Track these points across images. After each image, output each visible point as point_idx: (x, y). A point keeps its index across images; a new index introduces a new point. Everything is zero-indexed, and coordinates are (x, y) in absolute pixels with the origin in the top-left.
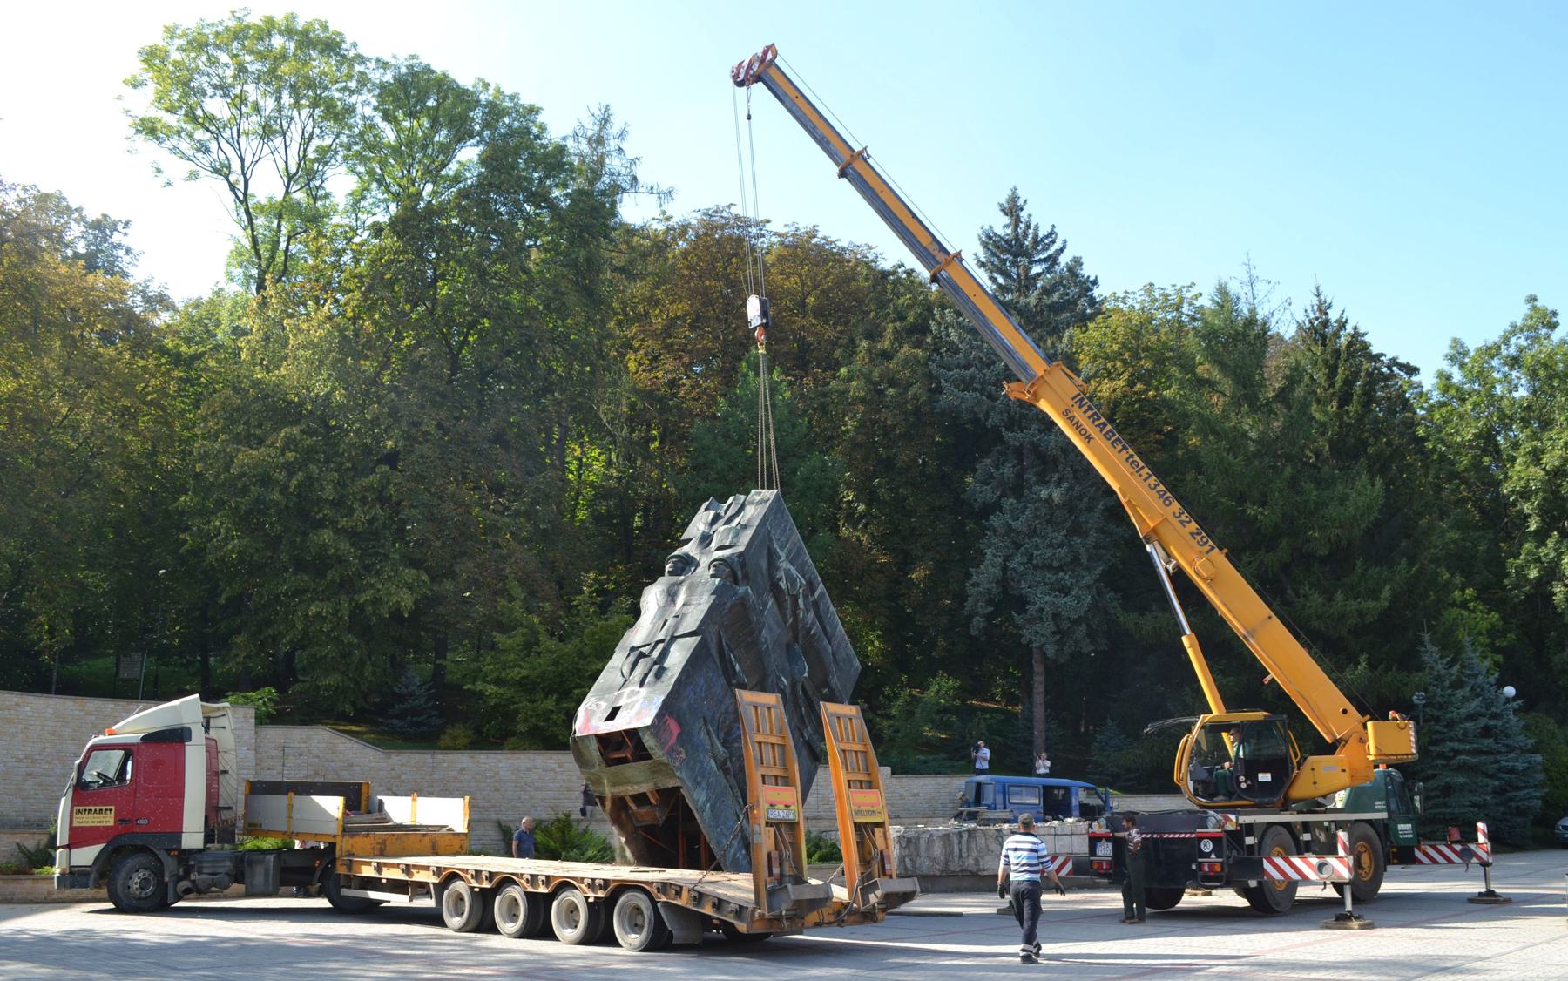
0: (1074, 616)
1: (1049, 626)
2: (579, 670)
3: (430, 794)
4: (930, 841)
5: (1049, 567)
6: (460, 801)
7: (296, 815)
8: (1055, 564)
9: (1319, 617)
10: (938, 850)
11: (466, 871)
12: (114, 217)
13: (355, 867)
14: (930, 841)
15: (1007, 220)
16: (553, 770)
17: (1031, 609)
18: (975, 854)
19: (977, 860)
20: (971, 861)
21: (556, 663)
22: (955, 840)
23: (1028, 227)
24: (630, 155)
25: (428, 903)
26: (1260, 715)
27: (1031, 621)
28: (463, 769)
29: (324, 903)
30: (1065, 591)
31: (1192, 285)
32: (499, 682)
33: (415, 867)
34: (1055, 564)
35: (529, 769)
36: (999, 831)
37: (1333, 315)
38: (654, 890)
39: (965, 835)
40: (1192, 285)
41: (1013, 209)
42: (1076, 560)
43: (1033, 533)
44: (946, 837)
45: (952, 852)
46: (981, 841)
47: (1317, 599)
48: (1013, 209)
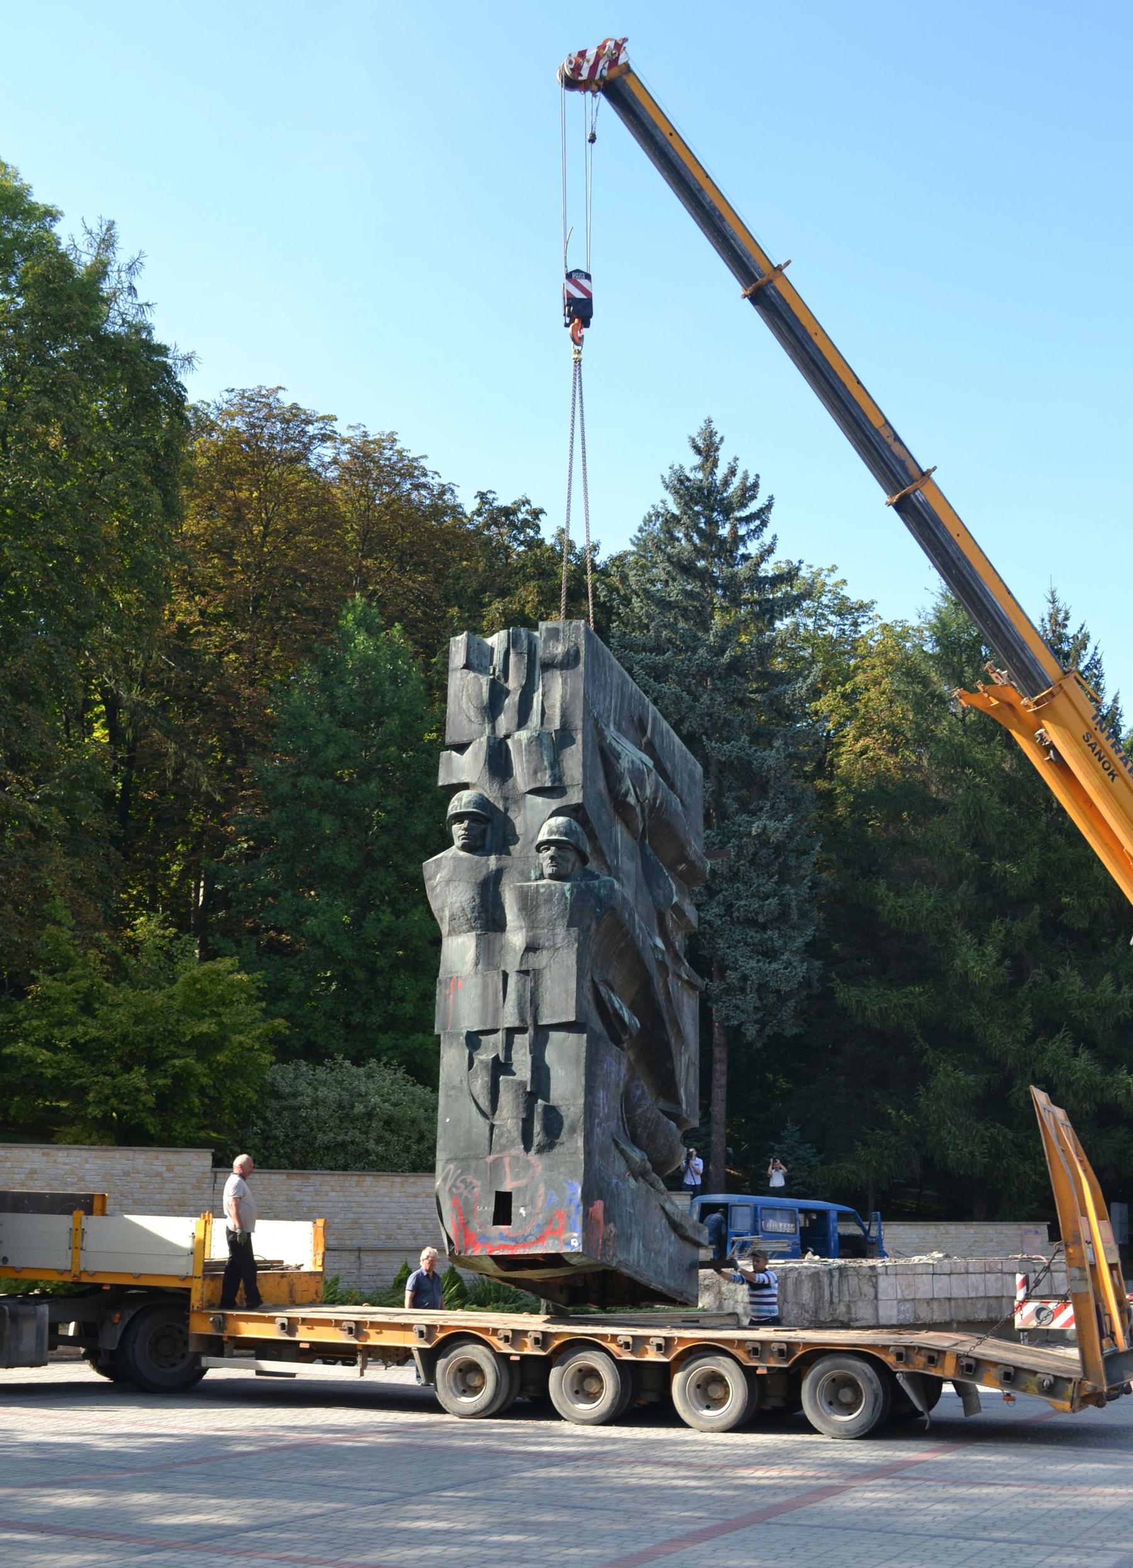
0: (785, 988)
1: (751, 1000)
2: (171, 1032)
3: (277, 1217)
4: (798, 1282)
5: (752, 923)
6: (308, 1225)
7: (89, 1243)
8: (761, 920)
9: (1081, 1005)
10: (806, 1295)
11: (495, 1331)
12: (866, 602)
13: (230, 1325)
14: (798, 1282)
15: (697, 460)
16: (159, 1175)
17: (732, 976)
18: (847, 1299)
19: (849, 1307)
20: (842, 1308)
21: (138, 1020)
22: (826, 1280)
23: (732, 472)
24: (141, 300)
25: (406, 1376)
26: (1053, 1118)
27: (728, 991)
28: (33, 1172)
29: (84, 1373)
30: (770, 954)
31: (833, 569)
32: (48, 1044)
33: (373, 1324)
34: (761, 920)
35: (126, 1174)
36: (873, 1268)
37: (1071, 630)
38: (890, 1360)
39: (836, 1274)
40: (833, 569)
41: (707, 450)
42: (784, 913)
43: (734, 876)
44: (815, 1276)
45: (821, 1297)
46: (853, 1281)
47: (1077, 981)
48: (708, 449)
